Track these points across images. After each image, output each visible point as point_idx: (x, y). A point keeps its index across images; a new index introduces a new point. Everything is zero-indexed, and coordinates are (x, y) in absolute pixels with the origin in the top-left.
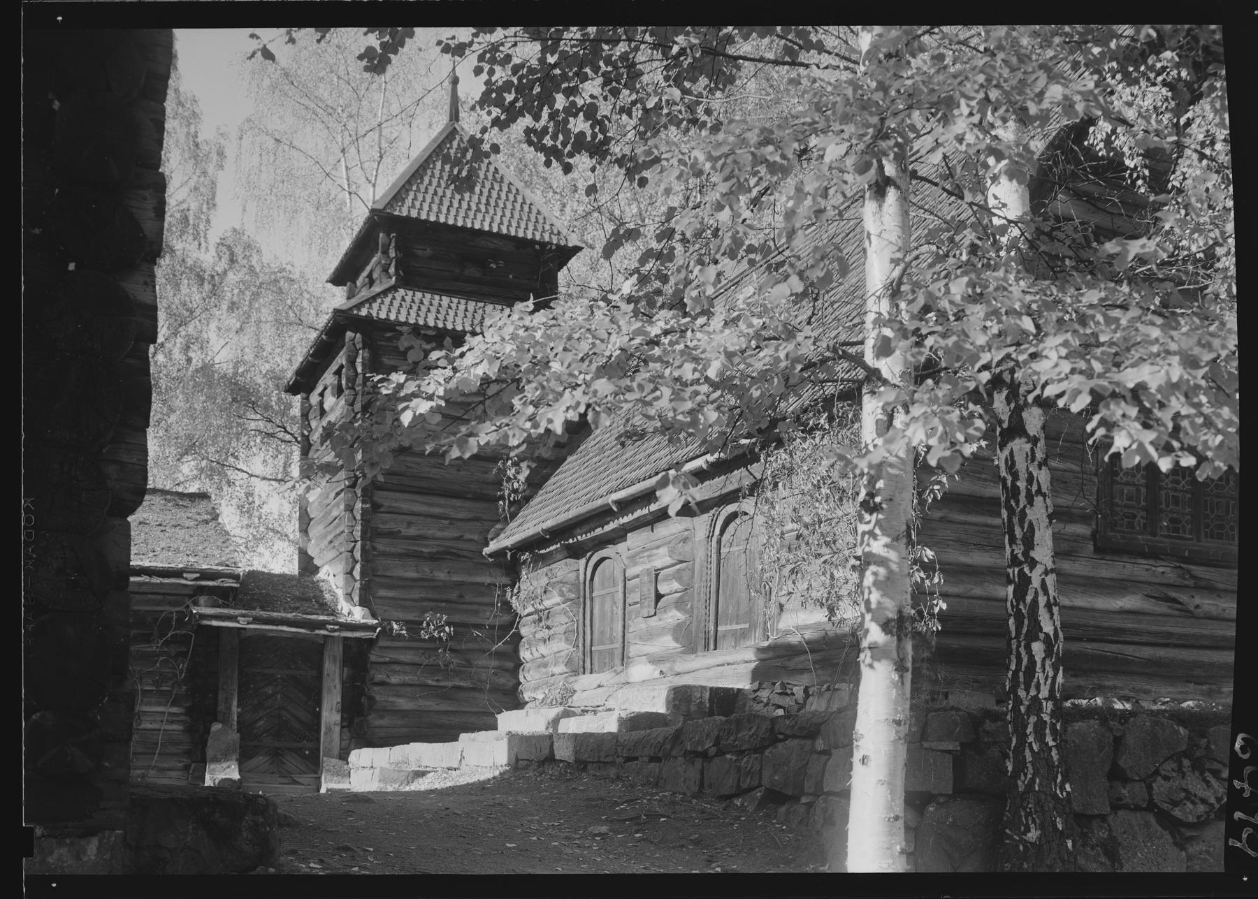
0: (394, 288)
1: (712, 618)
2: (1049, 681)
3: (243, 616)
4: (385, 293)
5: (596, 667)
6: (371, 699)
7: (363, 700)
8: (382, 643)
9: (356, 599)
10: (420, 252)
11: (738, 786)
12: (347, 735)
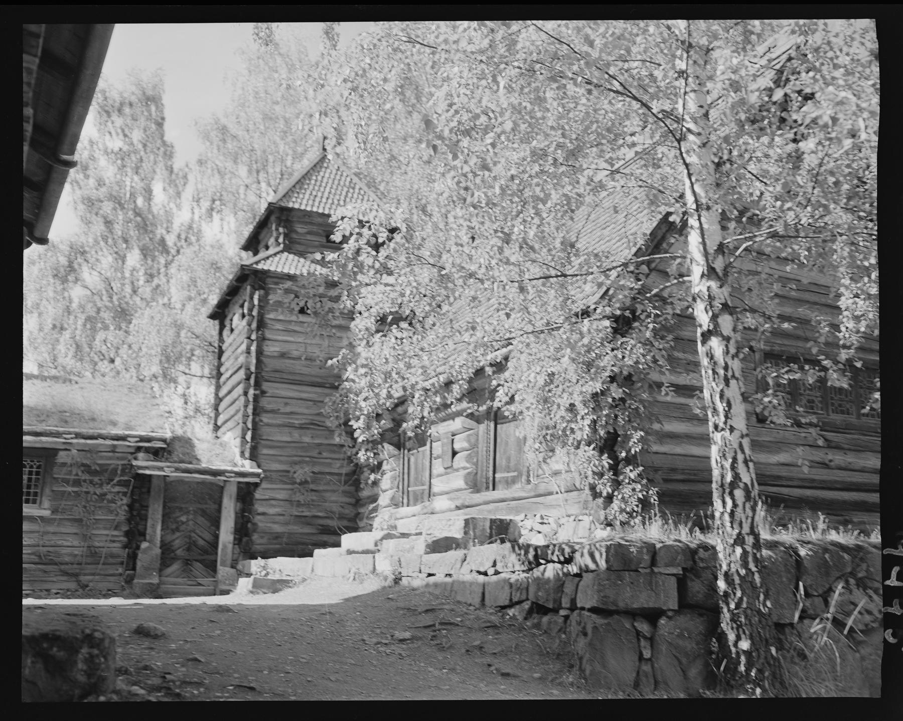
0: (282, 252)
1: (491, 469)
2: (750, 520)
3: (168, 467)
4: (275, 254)
5: (411, 502)
6: (255, 524)
7: (249, 525)
8: (264, 485)
9: (247, 455)
10: (299, 230)
11: (511, 600)
12: (237, 550)
